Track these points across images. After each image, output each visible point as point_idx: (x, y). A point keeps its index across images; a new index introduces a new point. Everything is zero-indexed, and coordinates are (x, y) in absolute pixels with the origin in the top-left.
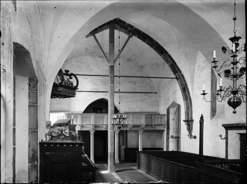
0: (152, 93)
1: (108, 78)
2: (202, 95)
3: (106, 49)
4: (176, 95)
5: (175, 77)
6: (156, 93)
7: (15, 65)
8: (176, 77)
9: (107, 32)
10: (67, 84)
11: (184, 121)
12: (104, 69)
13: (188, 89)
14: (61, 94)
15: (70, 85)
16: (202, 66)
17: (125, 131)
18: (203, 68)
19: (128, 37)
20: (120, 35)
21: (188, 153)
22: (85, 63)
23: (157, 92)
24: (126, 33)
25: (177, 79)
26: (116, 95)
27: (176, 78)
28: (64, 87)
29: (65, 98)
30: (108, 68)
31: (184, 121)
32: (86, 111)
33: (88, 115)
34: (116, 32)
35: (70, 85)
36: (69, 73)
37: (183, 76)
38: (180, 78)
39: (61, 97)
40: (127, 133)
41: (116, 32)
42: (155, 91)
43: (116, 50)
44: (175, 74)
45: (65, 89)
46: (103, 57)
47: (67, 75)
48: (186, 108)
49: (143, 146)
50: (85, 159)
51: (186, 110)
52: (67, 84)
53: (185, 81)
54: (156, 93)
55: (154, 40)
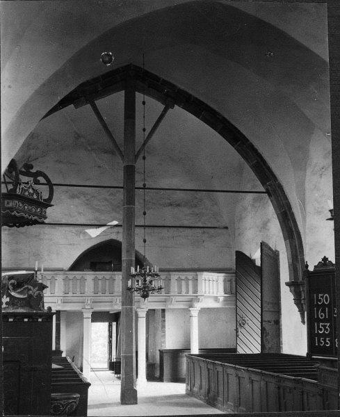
0: (216, 228)
1: (120, 195)
2: (329, 221)
3: (119, 135)
4: (269, 230)
5: (264, 191)
6: (226, 228)
7: (80, 350)
8: (267, 189)
9: (119, 98)
10: (27, 193)
11: (287, 284)
12: (119, 178)
13: (292, 214)
14: (13, 214)
15: (35, 197)
16: (321, 166)
17: (165, 377)
18: (323, 170)
19: (162, 107)
20: (149, 106)
21: (299, 356)
22: (73, 164)
23: (227, 225)
24: (158, 99)
25: (270, 195)
26: (139, 234)
27: (267, 192)
28: (21, 198)
29: (23, 226)
30: (121, 174)
31: (287, 284)
32: (76, 267)
33: (77, 274)
34: (139, 97)
35: (35, 197)
36: (34, 171)
37: (280, 187)
38: (274, 191)
39: (14, 225)
40: (164, 316)
41: (139, 97)
42: (224, 224)
43: (140, 137)
44: (263, 184)
45: (23, 204)
46: (112, 153)
47: (28, 174)
48: (290, 256)
49: (201, 342)
50: (74, 381)
51: (291, 261)
52: (27, 193)
53: (286, 198)
54: (226, 228)
55: (219, 114)
